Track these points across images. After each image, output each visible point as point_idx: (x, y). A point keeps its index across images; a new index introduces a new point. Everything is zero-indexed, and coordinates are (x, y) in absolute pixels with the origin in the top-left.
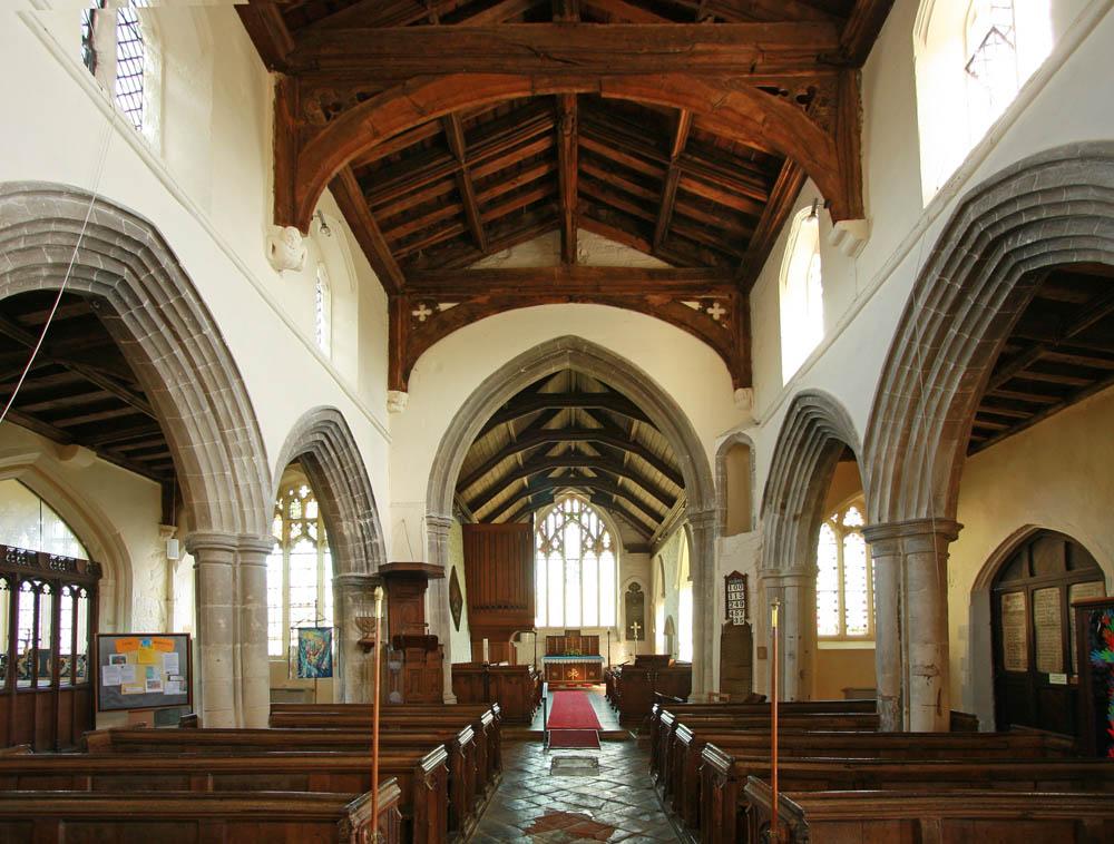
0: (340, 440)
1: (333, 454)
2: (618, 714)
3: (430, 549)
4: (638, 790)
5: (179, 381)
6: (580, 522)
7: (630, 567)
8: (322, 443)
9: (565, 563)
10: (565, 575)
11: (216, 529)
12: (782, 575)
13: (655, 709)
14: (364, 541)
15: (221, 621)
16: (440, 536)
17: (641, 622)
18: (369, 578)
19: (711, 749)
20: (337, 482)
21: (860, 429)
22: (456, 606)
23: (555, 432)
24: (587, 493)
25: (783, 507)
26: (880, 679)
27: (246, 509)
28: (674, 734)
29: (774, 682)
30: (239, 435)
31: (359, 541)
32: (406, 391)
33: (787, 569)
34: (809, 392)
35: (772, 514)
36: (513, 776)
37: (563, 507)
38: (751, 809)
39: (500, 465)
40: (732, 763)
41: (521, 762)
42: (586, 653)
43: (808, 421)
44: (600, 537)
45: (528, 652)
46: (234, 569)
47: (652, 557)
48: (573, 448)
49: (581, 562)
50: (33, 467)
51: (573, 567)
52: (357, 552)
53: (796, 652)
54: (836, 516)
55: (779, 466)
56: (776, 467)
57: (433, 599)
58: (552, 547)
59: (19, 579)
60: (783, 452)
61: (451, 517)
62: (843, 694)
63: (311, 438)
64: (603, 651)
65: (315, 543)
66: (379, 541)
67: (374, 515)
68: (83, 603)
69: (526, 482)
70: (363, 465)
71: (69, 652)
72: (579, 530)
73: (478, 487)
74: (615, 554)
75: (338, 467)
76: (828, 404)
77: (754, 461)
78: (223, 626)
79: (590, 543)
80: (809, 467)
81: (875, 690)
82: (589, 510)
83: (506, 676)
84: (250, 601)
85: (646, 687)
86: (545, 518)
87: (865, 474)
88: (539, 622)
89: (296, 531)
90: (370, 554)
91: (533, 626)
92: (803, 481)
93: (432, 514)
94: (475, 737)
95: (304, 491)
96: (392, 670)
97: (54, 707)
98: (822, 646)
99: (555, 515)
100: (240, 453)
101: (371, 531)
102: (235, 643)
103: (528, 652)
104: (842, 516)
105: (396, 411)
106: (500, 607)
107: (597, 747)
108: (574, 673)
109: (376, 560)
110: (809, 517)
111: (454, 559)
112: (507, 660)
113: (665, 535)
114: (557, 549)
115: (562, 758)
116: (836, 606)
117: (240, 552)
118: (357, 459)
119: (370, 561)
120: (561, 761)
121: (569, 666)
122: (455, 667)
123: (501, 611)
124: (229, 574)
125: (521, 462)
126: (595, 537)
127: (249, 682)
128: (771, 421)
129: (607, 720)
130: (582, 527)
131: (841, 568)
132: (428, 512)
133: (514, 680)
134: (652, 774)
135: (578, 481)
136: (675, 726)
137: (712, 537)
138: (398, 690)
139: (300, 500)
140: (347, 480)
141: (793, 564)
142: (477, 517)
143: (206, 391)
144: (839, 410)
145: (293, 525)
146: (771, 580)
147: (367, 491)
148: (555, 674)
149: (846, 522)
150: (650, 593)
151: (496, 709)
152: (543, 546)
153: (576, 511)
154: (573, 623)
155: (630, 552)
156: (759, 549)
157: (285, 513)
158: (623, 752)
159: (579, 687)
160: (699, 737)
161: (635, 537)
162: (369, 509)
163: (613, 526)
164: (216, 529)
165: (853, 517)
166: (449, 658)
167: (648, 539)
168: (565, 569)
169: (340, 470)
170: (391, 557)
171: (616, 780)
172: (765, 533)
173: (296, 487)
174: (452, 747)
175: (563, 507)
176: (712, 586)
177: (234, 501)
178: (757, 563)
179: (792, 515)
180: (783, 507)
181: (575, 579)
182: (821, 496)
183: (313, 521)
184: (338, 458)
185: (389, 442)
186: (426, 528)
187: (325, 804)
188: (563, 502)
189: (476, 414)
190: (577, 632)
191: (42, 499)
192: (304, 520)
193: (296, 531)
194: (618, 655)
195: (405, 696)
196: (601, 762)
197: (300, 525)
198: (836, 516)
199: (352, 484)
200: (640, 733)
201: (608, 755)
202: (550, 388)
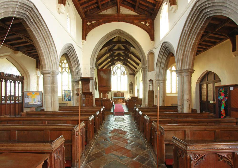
1: (71, 53)
2: (128, 109)
4: (132, 124)
5: (39, 37)
6: (120, 69)
8: (69, 51)
11: (47, 69)
13: (135, 108)
15: (48, 89)
16: (93, 71)
17: (132, 90)
19: (146, 116)
20: (72, 59)
21: (175, 49)
22: (96, 86)
23: (116, 49)
24: (122, 63)
25: (160, 66)
27: (53, 65)
29: (158, 102)
30: (52, 49)
32: (86, 40)
33: (161, 79)
39: (105, 56)
42: (122, 96)
43: (165, 48)
44: (124, 72)
45: (110, 96)
46: (51, 78)
47: (134, 76)
50: (9, 56)
54: (170, 68)
56: (159, 57)
57: (91, 85)
59: (7, 79)
60: (160, 54)
61: (95, 67)
64: (125, 96)
66: (80, 72)
67: (79, 67)
68: (20, 85)
69: (110, 60)
70: (77, 56)
71: (18, 95)
73: (100, 61)
75: (72, 56)
76: (169, 44)
78: (49, 90)
79: (122, 73)
80: (165, 58)
82: (122, 66)
84: (54, 85)
85: (133, 103)
86: (114, 68)
88: (112, 89)
89: (64, 70)
90: (78, 75)
92: (164, 60)
95: (65, 61)
96: (83, 100)
97: (15, 107)
98: (167, 95)
100: (52, 53)
101: (79, 70)
102: (51, 93)
103: (110, 96)
105: (84, 45)
107: (124, 115)
108: (119, 100)
111: (95, 76)
113: (137, 72)
115: (117, 118)
117: (52, 74)
121: (118, 99)
122: (96, 99)
123: (105, 87)
124: (50, 79)
125: (109, 56)
127: (54, 102)
129: (126, 110)
130: (121, 70)
131: (171, 79)
132: (90, 66)
133: (107, 102)
135: (120, 60)
139: (64, 63)
140: (74, 59)
142: (100, 67)
143: (45, 39)
145: (63, 69)
147: (78, 61)
148: (115, 101)
151: (104, 107)
152: (113, 74)
153: (120, 66)
156: (155, 75)
158: (129, 117)
159: (120, 103)
161: (131, 72)
163: (127, 70)
164: (47, 69)
165: (174, 68)
166: (94, 97)
167: (134, 72)
171: (127, 122)
173: (64, 61)
174: (95, 115)
177: (51, 63)
178: (155, 77)
179: (162, 67)
180: (160, 66)
181: (120, 80)
182: (168, 64)
183: (67, 68)
184: (72, 54)
185: (82, 51)
186: (90, 69)
188: (117, 64)
189: (100, 45)
190: (120, 92)
191: (11, 63)
192: (65, 68)
193: (64, 70)
194: (128, 96)
195: (86, 105)
196: (124, 119)
197: (64, 69)
198: (170, 68)
202: (115, 40)
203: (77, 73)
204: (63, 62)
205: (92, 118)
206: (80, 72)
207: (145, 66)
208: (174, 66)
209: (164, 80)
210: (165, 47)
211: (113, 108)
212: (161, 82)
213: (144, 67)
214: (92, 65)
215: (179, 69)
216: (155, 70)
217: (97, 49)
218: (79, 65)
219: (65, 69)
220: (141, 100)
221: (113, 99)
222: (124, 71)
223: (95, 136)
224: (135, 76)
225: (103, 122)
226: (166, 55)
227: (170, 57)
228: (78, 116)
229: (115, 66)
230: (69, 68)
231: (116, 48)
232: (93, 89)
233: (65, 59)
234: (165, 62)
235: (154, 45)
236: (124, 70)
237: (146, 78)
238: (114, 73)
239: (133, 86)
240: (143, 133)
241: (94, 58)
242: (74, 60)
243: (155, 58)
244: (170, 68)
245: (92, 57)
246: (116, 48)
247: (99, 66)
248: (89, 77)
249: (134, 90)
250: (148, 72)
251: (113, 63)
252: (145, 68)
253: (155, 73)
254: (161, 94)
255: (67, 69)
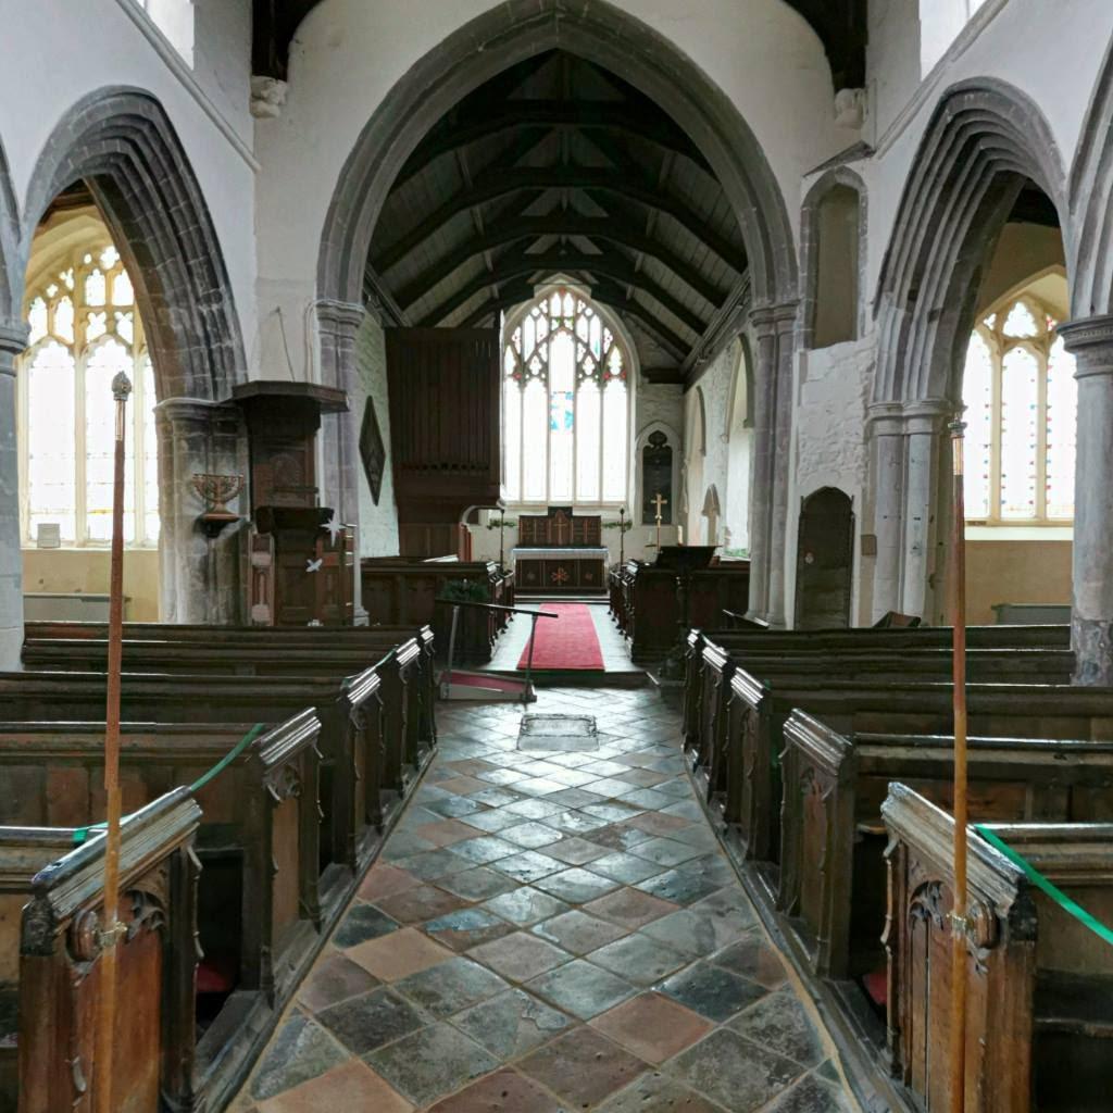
0: (161, 156)
1: (148, 181)
3: (325, 362)
6: (573, 332)
7: (651, 406)
8: (128, 160)
9: (549, 398)
10: (549, 418)
12: (905, 414)
13: (692, 638)
14: (208, 343)
16: (341, 340)
17: (667, 495)
18: (218, 408)
19: (798, 718)
20: (158, 234)
21: (1066, 143)
22: (373, 462)
24: (584, 282)
25: (913, 296)
26: (1078, 591)
28: (727, 688)
29: (885, 590)
31: (198, 343)
33: (915, 404)
34: (970, 85)
35: (894, 308)
36: (454, 749)
37: (548, 306)
38: (896, 849)
39: (446, 227)
40: (848, 752)
41: (469, 723)
43: (962, 142)
44: (605, 357)
45: (491, 543)
47: (686, 390)
48: (565, 205)
49: (575, 399)
51: (562, 405)
52: (196, 362)
53: (925, 544)
54: (993, 318)
55: (909, 223)
56: (903, 226)
57: (331, 457)
58: (530, 372)
60: (917, 200)
61: (359, 307)
62: (994, 615)
63: (105, 148)
65: (130, 349)
66: (233, 344)
67: (226, 297)
70: (204, 205)
72: (571, 345)
73: (410, 266)
74: (628, 385)
75: (159, 206)
76: (1006, 103)
77: (865, 217)
79: (589, 367)
80: (960, 223)
81: (1069, 608)
82: (589, 312)
83: (407, 577)
85: (676, 598)
86: (520, 323)
87: (1070, 225)
88: (508, 492)
89: (96, 326)
90: (218, 366)
91: (497, 496)
92: (946, 252)
93: (326, 300)
94: (381, 690)
95: (110, 256)
96: (255, 568)
98: (971, 534)
99: (535, 319)
101: (220, 326)
103: (491, 543)
104: (1002, 317)
105: (266, 115)
106: (445, 466)
109: (229, 378)
110: (956, 315)
111: (366, 386)
112: (455, 552)
113: (709, 355)
114: (539, 376)
116: (987, 469)
118: (194, 195)
119: (218, 379)
120: (536, 723)
122: (371, 564)
123: (446, 473)
126: (598, 358)
128: (897, 143)
129: (615, 655)
130: (577, 340)
131: (998, 404)
132: (320, 296)
134: (687, 750)
135: (564, 261)
136: (729, 671)
137: (791, 349)
138: (266, 602)
139: (104, 272)
140: (176, 231)
141: (924, 395)
142: (409, 317)
144: (1025, 109)
145: (91, 316)
146: (886, 423)
147: (213, 252)
149: (1010, 329)
150: (682, 448)
151: (427, 635)
152: (516, 369)
153: (569, 313)
154: (561, 496)
155: (652, 382)
156: (870, 369)
157: (76, 296)
160: (776, 693)
161: (660, 357)
162: (217, 286)
163: (626, 338)
165: (1021, 321)
167: (681, 361)
168: (549, 408)
169: (163, 214)
170: (256, 371)
172: (880, 342)
173: (96, 250)
174: (333, 708)
175: (548, 306)
176: (787, 432)
178: (866, 392)
179: (928, 308)
180: (913, 296)
181: (565, 423)
182: (976, 280)
183: (125, 310)
186: (316, 325)
187: (17, 853)
188: (548, 297)
189: (400, 126)
190: (567, 510)
192: (110, 310)
193: (96, 326)
197: (103, 316)
198: (993, 318)
199: (185, 240)
200: (662, 676)
201: (612, 713)
202: (531, 90)
203: (206, 353)
204: (88, 259)
205: (365, 685)
206: (228, 343)
207: (781, 299)
208: (1025, 302)
209: (946, 418)
210: (964, 127)
211: (322, 938)
212: (914, 426)
213: (770, 310)
214: (335, 290)
215: (1092, 308)
216: (869, 324)
217: (374, 156)
218: (222, 288)
219: (112, 324)
220: (743, 566)
221: (511, 564)
222: (602, 348)
223: (329, 905)
224: (693, 391)
225: (414, 762)
226: (964, 204)
227: (996, 232)
228: (126, 755)
229: (535, 312)
230: (137, 311)
231: (540, 208)
232: (345, 482)
233: (102, 236)
234: (953, 261)
235: (858, 123)
236: (603, 342)
237: (789, 397)
238: (522, 372)
239: (669, 464)
240: (767, 865)
241: (352, 228)
242: (179, 239)
243: (865, 232)
244: (990, 321)
245: (338, 219)
246: (540, 208)
247: (403, 307)
248: (305, 385)
249: (680, 496)
250: (801, 349)
251: (519, 292)
252: (777, 314)
253: (865, 360)
254: (911, 523)
255: (130, 315)
